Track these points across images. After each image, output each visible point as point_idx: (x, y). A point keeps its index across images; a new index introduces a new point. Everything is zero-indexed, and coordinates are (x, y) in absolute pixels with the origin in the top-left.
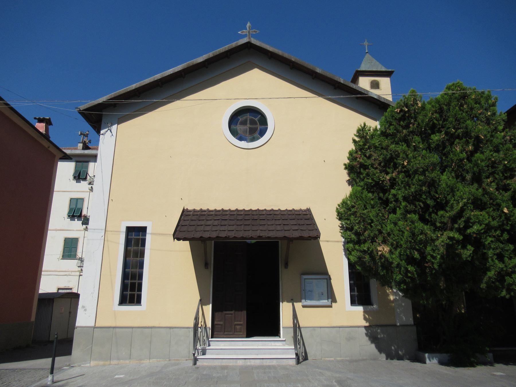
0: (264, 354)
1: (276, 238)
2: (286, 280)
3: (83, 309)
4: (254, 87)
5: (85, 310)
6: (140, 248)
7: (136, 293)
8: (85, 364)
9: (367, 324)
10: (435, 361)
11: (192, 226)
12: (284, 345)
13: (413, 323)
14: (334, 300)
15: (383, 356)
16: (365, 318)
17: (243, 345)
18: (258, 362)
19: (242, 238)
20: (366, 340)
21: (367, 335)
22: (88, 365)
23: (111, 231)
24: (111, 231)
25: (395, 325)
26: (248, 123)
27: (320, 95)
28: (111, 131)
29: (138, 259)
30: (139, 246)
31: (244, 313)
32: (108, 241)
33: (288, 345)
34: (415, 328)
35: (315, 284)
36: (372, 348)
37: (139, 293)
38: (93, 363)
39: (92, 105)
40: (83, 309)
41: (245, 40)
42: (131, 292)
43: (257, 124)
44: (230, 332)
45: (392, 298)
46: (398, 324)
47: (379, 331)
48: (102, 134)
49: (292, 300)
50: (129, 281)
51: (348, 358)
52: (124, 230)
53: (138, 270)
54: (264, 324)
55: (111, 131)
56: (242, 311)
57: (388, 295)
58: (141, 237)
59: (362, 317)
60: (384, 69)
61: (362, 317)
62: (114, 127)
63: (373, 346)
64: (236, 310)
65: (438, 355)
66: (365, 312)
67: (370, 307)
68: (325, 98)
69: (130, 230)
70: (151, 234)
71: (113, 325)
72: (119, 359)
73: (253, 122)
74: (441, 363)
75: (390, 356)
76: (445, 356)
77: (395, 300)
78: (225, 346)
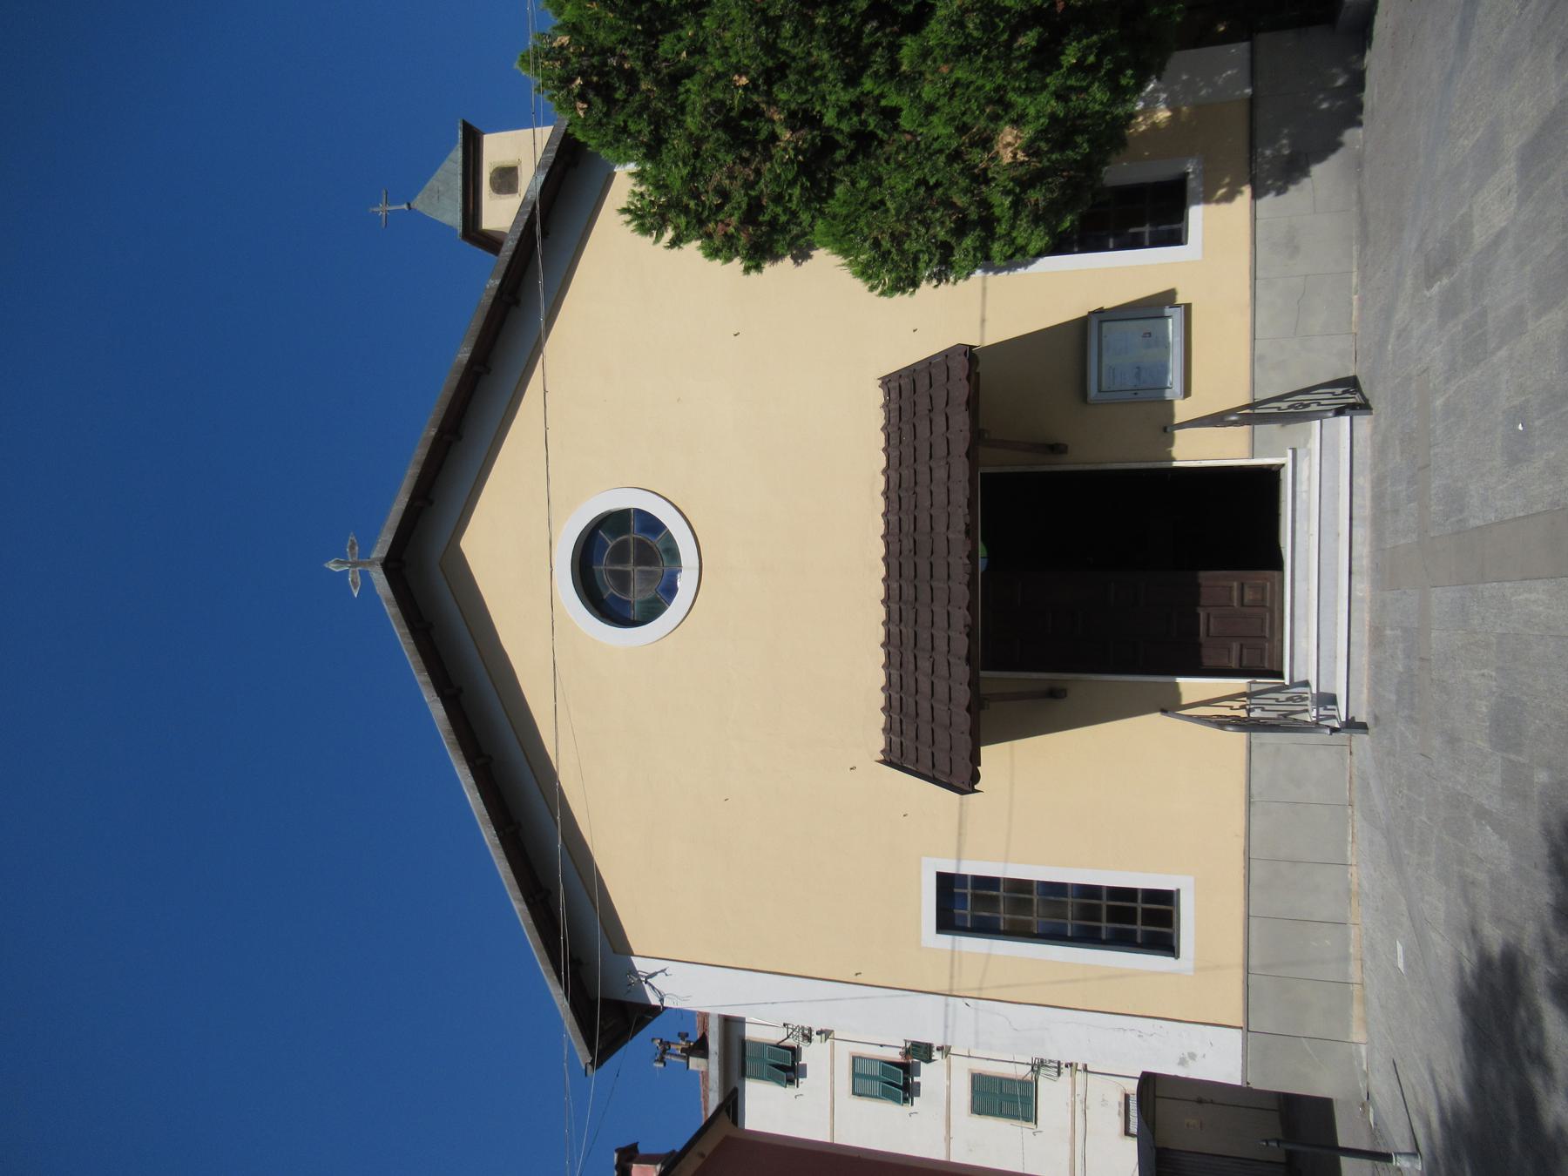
1: (971, 481)
2: (1102, 448)
4: (514, 549)
5: (1193, 1056)
6: (1001, 893)
7: (1140, 906)
9: (1247, 190)
11: (936, 737)
12: (1309, 453)
13: (1245, 45)
14: (1168, 297)
15: (1351, 136)
16: (1229, 198)
17: (1307, 579)
21: (1281, 191)
22: (1363, 1049)
24: (952, 977)
25: (1252, 101)
27: (537, 350)
28: (652, 976)
29: (1035, 898)
31: (1203, 576)
32: (980, 989)
34: (1263, 38)
35: (1116, 357)
38: (1358, 1035)
41: (379, 578)
44: (1263, 620)
45: (1163, 115)
46: (1248, 91)
47: (1268, 152)
50: (1105, 925)
52: (946, 940)
53: (1070, 900)
54: (1239, 517)
55: (652, 976)
56: (1198, 586)
58: (969, 891)
59: (1224, 207)
60: (457, 154)
61: (1224, 207)
62: (640, 964)
63: (1316, 170)
66: (1207, 199)
67: (1193, 184)
69: (946, 923)
70: (959, 859)
71: (1237, 975)
72: (1346, 958)
73: (620, 554)
75: (1352, 114)
78: (1307, 637)
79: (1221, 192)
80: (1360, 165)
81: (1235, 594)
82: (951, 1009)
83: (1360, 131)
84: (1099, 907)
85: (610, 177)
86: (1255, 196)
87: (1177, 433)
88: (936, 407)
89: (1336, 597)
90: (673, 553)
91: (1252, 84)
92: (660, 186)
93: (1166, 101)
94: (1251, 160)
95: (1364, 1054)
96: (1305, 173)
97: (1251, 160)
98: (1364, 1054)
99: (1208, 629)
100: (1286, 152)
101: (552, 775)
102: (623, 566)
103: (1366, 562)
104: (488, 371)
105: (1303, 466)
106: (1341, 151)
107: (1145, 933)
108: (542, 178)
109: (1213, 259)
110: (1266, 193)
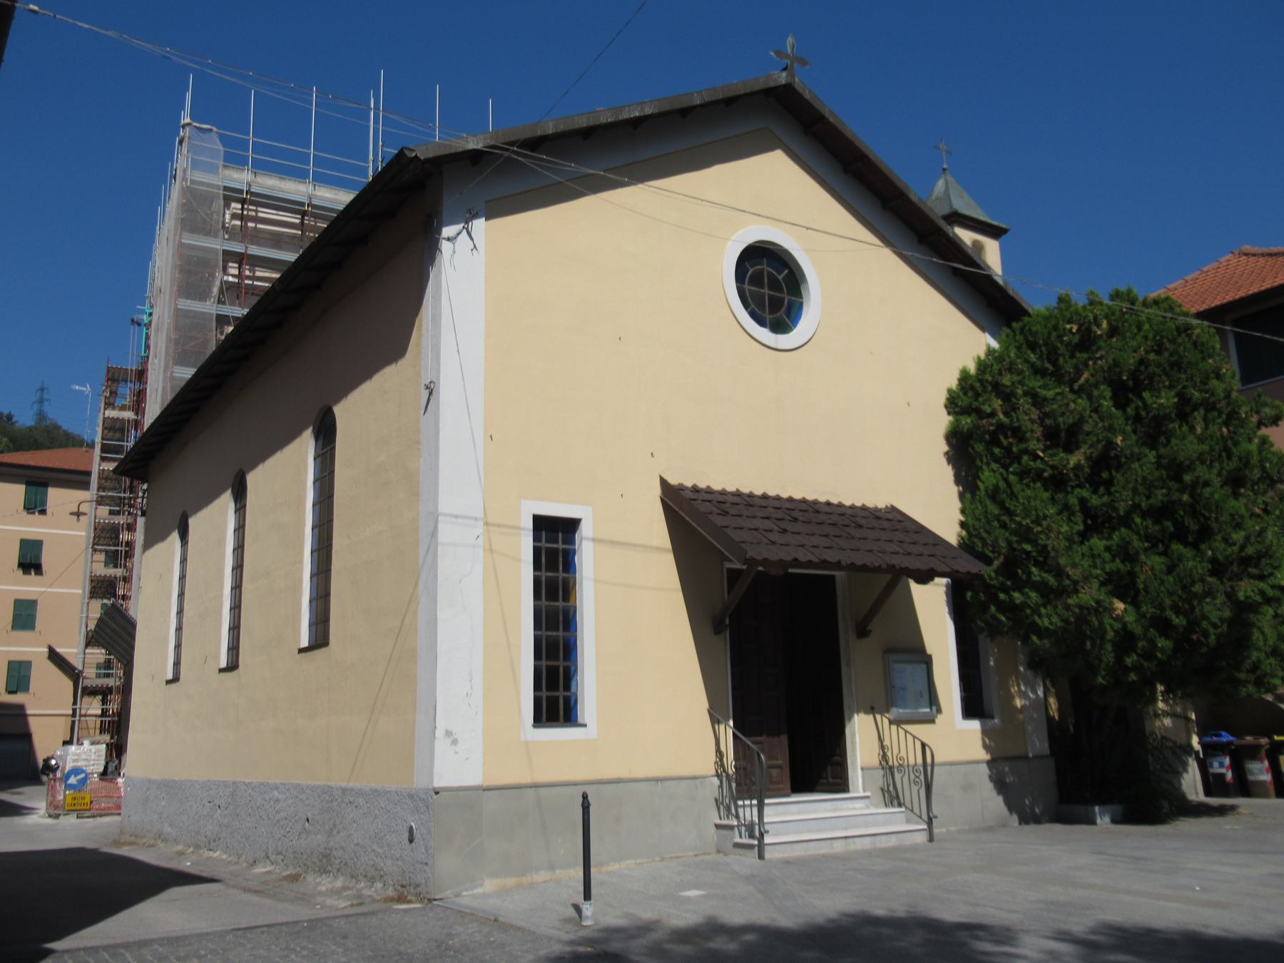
3: (449, 741)
4: (772, 194)
6: (561, 575)
7: (561, 694)
9: (988, 757)
10: (1107, 819)
11: (699, 523)
12: (868, 807)
14: (939, 711)
15: (1015, 817)
16: (985, 746)
20: (988, 788)
21: (990, 777)
23: (499, 526)
24: (499, 526)
25: (1027, 757)
26: (770, 284)
27: (887, 242)
28: (469, 234)
29: (560, 604)
35: (907, 673)
38: (489, 885)
41: (783, 78)
47: (1007, 769)
48: (448, 239)
49: (872, 710)
52: (529, 524)
53: (561, 633)
54: (818, 768)
55: (469, 234)
57: (1012, 698)
58: (561, 546)
59: (980, 743)
60: (983, 217)
63: (1000, 799)
65: (1110, 807)
66: (985, 732)
67: (990, 722)
68: (895, 252)
70: (594, 540)
71: (526, 779)
72: (552, 868)
73: (774, 284)
74: (1114, 821)
76: (1118, 808)
83: (1016, 823)
84: (557, 659)
88: (880, 548)
90: (761, 322)
92: (1273, 454)
95: (475, 891)
98: (475, 891)
102: (770, 284)
104: (884, 207)
109: (957, 738)
110: (990, 769)
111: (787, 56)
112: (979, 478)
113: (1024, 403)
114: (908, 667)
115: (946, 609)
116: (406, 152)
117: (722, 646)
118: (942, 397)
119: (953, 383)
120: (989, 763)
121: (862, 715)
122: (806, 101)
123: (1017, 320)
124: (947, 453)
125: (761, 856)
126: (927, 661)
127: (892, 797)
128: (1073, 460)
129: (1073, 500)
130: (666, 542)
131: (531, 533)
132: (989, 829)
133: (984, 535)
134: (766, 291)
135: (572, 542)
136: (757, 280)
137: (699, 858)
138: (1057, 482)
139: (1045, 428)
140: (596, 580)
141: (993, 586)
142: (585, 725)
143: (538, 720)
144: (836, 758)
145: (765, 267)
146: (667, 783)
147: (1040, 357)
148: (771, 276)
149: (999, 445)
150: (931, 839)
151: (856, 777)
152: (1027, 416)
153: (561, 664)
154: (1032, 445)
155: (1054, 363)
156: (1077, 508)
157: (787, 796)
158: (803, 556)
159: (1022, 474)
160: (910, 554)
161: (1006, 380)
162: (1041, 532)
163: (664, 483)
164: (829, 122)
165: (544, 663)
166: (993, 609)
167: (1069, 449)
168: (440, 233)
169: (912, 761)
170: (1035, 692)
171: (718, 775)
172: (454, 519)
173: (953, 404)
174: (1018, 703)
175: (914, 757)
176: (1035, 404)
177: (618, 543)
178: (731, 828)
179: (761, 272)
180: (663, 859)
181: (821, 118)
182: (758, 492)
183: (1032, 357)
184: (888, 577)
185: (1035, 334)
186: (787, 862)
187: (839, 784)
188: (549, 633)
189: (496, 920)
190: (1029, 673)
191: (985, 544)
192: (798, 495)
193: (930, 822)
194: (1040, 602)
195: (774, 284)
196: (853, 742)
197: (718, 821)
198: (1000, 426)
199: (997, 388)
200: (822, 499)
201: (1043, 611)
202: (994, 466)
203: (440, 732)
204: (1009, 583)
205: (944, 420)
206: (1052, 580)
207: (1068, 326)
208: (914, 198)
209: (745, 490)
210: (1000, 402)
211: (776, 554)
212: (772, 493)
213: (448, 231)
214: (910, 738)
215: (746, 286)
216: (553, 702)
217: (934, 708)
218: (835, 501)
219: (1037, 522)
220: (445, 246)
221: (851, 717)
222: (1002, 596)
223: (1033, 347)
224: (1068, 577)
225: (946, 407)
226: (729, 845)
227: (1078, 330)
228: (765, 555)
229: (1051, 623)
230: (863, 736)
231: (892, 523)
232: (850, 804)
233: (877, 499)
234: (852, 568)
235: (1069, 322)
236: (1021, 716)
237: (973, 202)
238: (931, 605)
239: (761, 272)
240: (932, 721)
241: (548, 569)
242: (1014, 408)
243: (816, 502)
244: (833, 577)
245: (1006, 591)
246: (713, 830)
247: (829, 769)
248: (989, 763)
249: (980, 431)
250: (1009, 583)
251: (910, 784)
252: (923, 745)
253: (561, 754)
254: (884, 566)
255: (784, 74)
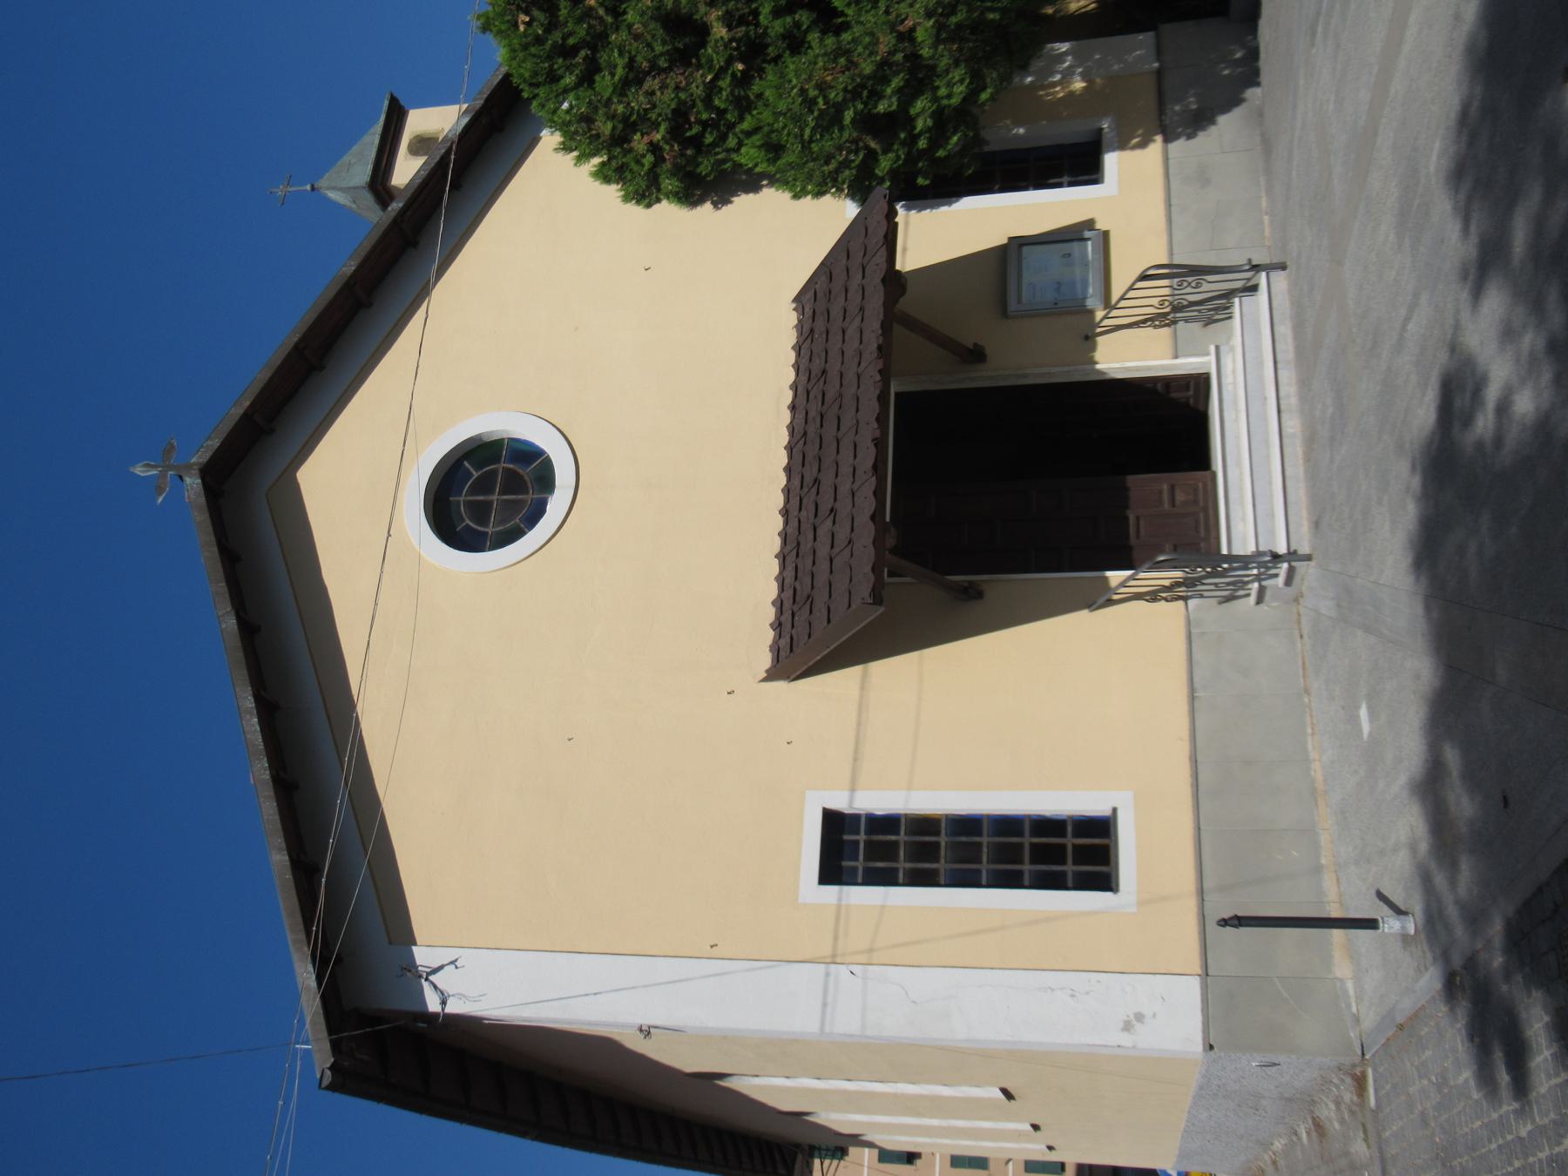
0: (1261, 379)
1: (883, 398)
2: (1022, 359)
3: (1137, 1026)
4: (358, 483)
5: (1140, 1017)
6: (902, 837)
8: (1345, 992)
9: (1159, 138)
12: (1232, 349)
13: (1151, 34)
14: (1089, 224)
15: (1252, 93)
16: (1143, 145)
17: (1239, 464)
18: (1287, 375)
19: (881, 420)
20: (1207, 141)
21: (1190, 137)
22: (1350, 986)
24: (836, 938)
25: (1159, 73)
26: (486, 494)
27: (424, 292)
28: (435, 971)
29: (943, 840)
30: (896, 844)
31: (1133, 480)
32: (871, 950)
33: (1229, 338)
34: (1166, 28)
35: (1037, 275)
36: (1227, 123)
37: (1069, 829)
39: (322, 1020)
40: (1137, 1026)
41: (193, 482)
42: (1070, 853)
43: (494, 473)
44: (1197, 522)
45: (1078, 85)
46: (1156, 65)
47: (1177, 108)
48: (444, 1003)
50: (1027, 868)
51: (1262, 180)
52: (832, 891)
53: (985, 840)
54: (1170, 424)
56: (1127, 489)
57: (1072, 93)
58: (862, 837)
59: (1138, 154)
60: (378, 127)
61: (1138, 152)
62: (423, 956)
63: (1222, 120)
64: (1127, 507)
66: (1122, 145)
69: (833, 871)
70: (853, 790)
71: (1191, 904)
72: (1318, 870)
73: (484, 485)
75: (1251, 76)
77: (1084, 77)
78: (1244, 520)
79: (1135, 141)
80: (1261, 114)
81: (1166, 497)
82: (832, 979)
85: (535, 140)
86: (1167, 140)
87: (1100, 339)
88: (853, 306)
89: (1268, 456)
90: (537, 512)
91: (1158, 60)
93: (1081, 74)
94: (1161, 111)
95: (1351, 992)
96: (1212, 121)
97: (1161, 111)
98: (1351, 992)
99: (1138, 532)
100: (1194, 107)
101: (352, 706)
102: (486, 494)
103: (1294, 401)
105: (1227, 362)
106: (1244, 105)
107: (1076, 874)
108: (466, 120)
109: (1132, 201)
110: (1177, 137)
111: (162, 475)
112: (751, 169)
113: (638, 100)
114: (1027, 277)
115: (944, 209)
116: (326, 1082)
117: (1004, 586)
118: (635, 210)
119: (613, 191)
120: (1167, 140)
121: (1098, 355)
122: (223, 444)
123: (518, 92)
124: (716, 205)
125: (1308, 558)
126: (1018, 244)
127: (1216, 310)
128: (720, 31)
129: (778, 27)
130: (851, 674)
131: (846, 888)
132: (1267, 146)
133: (832, 166)
134: (495, 497)
135: (855, 818)
136: (481, 512)
137: (1305, 632)
138: (754, 52)
139: (672, 64)
140: (910, 787)
141: (908, 154)
142: (1115, 810)
143: (1104, 881)
144: (1159, 387)
145: (462, 498)
146: (1197, 685)
147: (570, 69)
148: (475, 490)
149: (701, 135)
150: (1283, 267)
151: (1188, 364)
152: (661, 95)
153: (1027, 840)
154: (697, 90)
155: (574, 50)
156: (789, 19)
157: (1214, 475)
158: (867, 504)
159: (744, 105)
160: (862, 309)
161: (606, 128)
162: (825, 97)
163: (765, 680)
164: (251, 406)
165: (1027, 868)
166: (941, 153)
167: (703, 31)
168: (436, 1015)
169: (1167, 291)
170: (1060, 58)
171: (1174, 322)
172: (829, 1009)
173: (645, 194)
174: (1078, 85)
175: (1160, 290)
176: (639, 82)
177: (856, 751)
178: (1262, 590)
179: (469, 504)
180: (1307, 691)
181: (247, 417)
182: (779, 522)
183: (569, 80)
184: (898, 330)
185: (535, 74)
186: (1316, 525)
187: (1199, 384)
188: (985, 859)
189: (1401, 1027)
190: (1037, 64)
191: (845, 164)
192: (782, 459)
193: (1256, 268)
194: (928, 95)
195: (484, 485)
196: (1137, 369)
197: (1252, 599)
198: (675, 133)
199: (619, 140)
200: (786, 417)
201: (943, 92)
202: (732, 142)
203: (1126, 1040)
204: (902, 136)
205: (667, 210)
206: (896, 82)
207: (522, 28)
208: (350, 268)
209: (776, 544)
210: (637, 137)
211: (866, 534)
212: (779, 500)
213: (433, 1005)
214: (1131, 294)
215: (490, 530)
216: (1083, 855)
217: (1087, 234)
218: (788, 396)
219: (810, 103)
220: (453, 1007)
221: (1100, 372)
222: (922, 144)
223: (553, 78)
224: (892, 53)
225: (649, 206)
226: (1291, 591)
227: (527, 13)
228: (868, 569)
229: (961, 81)
230: (1127, 354)
231: (821, 302)
232: (1227, 380)
233: (784, 326)
234: (885, 375)
235: (516, 26)
236: (1098, 80)
237: (355, 149)
238: (936, 235)
239: (469, 504)
240: (1106, 235)
241: (894, 857)
242: (643, 116)
243: (792, 429)
244: (897, 394)
245: (914, 138)
246: (1263, 607)
247: (1174, 395)
248: (1167, 140)
249: (683, 162)
250: (902, 136)
251: (1198, 292)
252: (1144, 277)
253: (1151, 851)
254: (880, 365)
255: (188, 480)
